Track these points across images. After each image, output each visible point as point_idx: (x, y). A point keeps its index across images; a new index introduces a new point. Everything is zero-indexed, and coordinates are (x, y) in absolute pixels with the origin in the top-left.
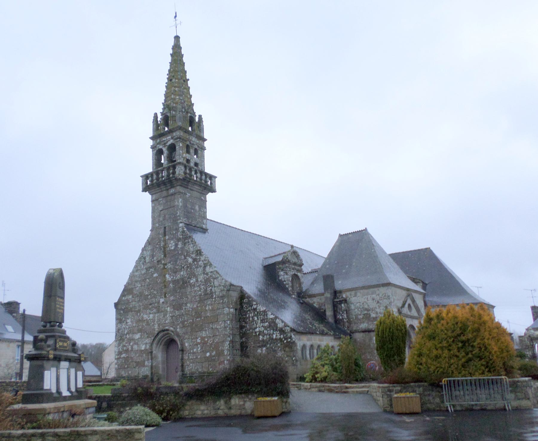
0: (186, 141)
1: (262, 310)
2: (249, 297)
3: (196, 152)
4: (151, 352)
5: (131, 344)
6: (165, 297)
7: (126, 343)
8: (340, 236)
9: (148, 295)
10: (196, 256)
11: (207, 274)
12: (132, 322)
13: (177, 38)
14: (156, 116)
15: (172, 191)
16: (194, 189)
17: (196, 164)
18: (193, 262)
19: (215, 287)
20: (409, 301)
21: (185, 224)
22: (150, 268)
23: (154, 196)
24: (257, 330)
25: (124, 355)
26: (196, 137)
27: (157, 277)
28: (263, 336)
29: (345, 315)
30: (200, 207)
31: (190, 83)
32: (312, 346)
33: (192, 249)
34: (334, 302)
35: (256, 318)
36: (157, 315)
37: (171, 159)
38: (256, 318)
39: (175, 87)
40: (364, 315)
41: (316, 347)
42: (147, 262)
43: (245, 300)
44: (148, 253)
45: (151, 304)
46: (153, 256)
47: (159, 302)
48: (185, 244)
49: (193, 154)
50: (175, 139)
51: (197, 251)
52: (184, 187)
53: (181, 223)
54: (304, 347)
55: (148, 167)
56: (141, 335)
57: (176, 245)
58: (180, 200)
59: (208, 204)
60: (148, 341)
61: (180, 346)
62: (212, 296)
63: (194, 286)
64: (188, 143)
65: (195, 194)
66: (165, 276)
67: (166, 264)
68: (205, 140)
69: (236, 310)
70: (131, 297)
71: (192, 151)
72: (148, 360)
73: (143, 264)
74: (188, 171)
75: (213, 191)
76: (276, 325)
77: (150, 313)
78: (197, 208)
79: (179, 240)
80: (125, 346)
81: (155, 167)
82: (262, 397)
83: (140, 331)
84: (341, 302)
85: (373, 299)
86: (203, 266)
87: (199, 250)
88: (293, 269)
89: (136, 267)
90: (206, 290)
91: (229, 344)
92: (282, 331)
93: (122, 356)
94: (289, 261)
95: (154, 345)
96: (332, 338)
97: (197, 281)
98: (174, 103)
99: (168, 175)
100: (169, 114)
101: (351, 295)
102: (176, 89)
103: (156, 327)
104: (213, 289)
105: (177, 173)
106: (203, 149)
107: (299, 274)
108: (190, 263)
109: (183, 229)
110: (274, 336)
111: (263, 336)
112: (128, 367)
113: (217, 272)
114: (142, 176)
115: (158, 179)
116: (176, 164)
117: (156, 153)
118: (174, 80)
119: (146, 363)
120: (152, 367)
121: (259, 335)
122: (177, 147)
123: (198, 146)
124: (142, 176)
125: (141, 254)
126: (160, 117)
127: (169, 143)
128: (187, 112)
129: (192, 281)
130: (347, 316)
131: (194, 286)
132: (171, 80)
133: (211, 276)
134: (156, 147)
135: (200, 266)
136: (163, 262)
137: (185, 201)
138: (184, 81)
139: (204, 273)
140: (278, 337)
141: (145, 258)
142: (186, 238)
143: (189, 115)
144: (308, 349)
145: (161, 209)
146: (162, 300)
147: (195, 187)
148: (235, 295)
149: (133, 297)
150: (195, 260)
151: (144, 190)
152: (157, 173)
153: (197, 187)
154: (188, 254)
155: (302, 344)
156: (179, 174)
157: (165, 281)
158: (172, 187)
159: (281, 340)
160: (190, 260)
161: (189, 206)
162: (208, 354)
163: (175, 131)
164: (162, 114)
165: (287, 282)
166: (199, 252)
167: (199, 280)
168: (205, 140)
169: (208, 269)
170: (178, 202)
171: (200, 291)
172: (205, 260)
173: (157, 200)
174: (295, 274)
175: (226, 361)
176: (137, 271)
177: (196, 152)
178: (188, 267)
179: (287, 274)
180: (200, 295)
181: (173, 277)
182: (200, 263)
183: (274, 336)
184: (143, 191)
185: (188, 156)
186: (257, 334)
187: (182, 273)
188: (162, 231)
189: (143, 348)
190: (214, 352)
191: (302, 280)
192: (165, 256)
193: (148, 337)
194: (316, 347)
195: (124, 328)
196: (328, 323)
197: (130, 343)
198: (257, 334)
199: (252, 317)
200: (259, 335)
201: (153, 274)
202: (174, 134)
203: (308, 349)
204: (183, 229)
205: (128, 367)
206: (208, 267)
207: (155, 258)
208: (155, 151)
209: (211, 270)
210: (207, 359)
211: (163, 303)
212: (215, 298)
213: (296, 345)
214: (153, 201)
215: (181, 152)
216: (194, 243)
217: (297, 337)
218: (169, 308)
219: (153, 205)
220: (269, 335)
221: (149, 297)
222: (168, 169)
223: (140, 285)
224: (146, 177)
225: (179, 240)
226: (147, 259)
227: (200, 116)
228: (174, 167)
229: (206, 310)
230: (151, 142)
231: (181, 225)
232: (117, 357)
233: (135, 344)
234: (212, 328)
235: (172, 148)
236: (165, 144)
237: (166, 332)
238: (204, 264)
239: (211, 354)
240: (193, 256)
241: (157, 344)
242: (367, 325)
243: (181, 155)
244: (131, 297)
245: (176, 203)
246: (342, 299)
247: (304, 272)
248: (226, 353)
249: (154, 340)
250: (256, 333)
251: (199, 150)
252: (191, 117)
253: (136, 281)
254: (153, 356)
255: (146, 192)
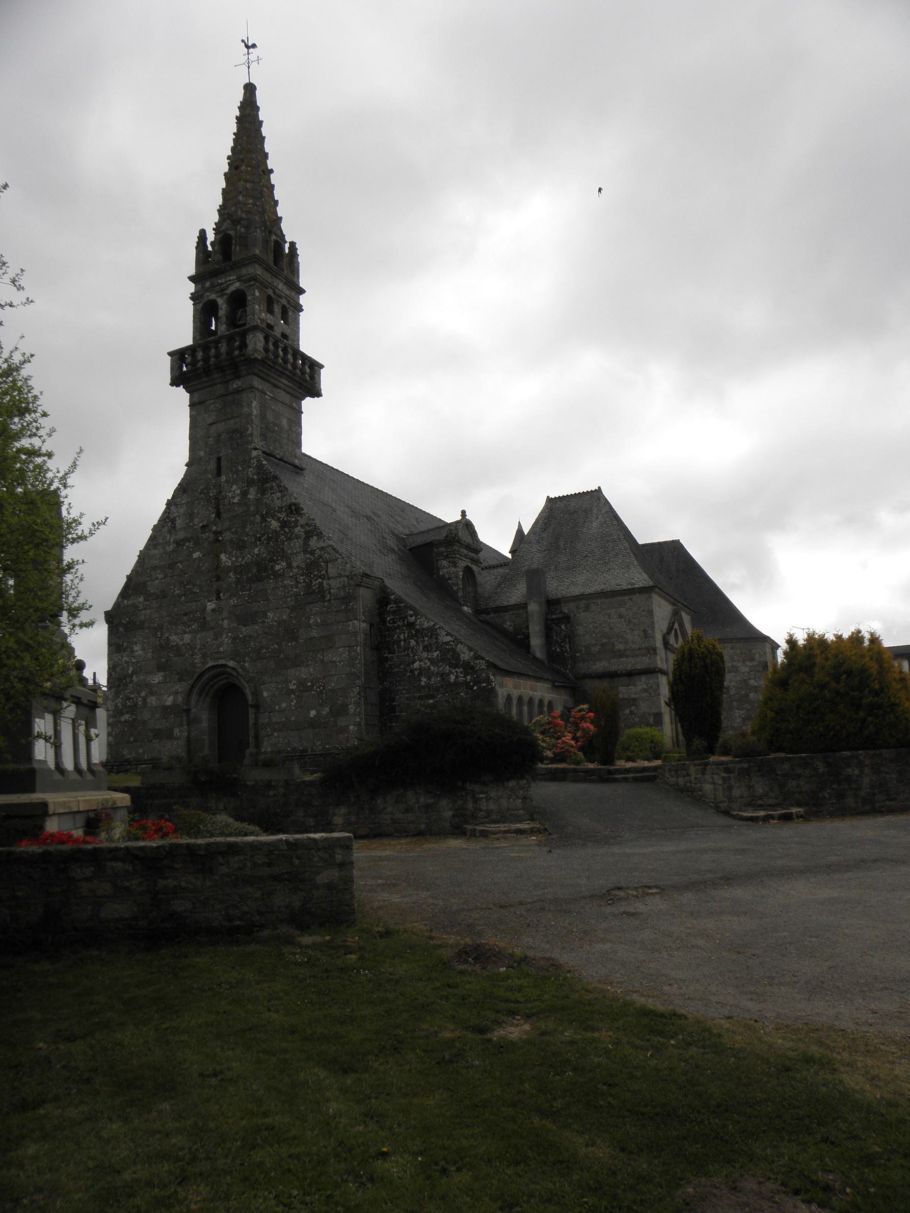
0: (267, 287)
1: (426, 625)
2: (399, 600)
3: (284, 315)
4: (188, 711)
5: (143, 694)
6: (218, 598)
7: (131, 693)
8: (549, 500)
9: (180, 596)
10: (287, 516)
11: (312, 553)
12: (143, 649)
13: (250, 89)
14: (202, 235)
15: (236, 384)
16: (281, 385)
17: (284, 336)
18: (282, 527)
19: (329, 579)
20: (676, 626)
21: (264, 452)
22: (187, 540)
23: (196, 395)
24: (416, 665)
25: (127, 717)
26: (285, 284)
27: (199, 558)
28: (429, 679)
29: (567, 646)
30: (290, 421)
31: (274, 179)
32: (520, 699)
33: (278, 503)
34: (546, 620)
35: (413, 643)
36: (199, 636)
37: (233, 320)
38: (413, 643)
39: (246, 181)
40: (602, 645)
41: (526, 699)
42: (178, 526)
43: (391, 607)
44: (182, 510)
45: (186, 614)
46: (191, 516)
47: (204, 609)
48: (263, 492)
49: (279, 316)
50: (245, 282)
51: (290, 506)
52: (262, 378)
53: (256, 449)
54: (509, 698)
55: (185, 338)
56: (165, 677)
57: (244, 494)
58: (255, 403)
59: (305, 419)
60: (181, 687)
61: (250, 698)
62: (323, 597)
63: (282, 575)
64: (270, 292)
65: (283, 396)
66: (217, 557)
67: (220, 533)
68: (302, 291)
69: (371, 625)
70: (141, 599)
71: (277, 309)
72: (181, 725)
73: (170, 532)
74: (271, 347)
75: (316, 393)
76: (456, 655)
77: (185, 633)
78: (285, 422)
79: (250, 483)
80: (129, 699)
81: (198, 337)
82: (236, 842)
83: (160, 668)
84: (559, 621)
85: (621, 616)
86: (303, 536)
87: (294, 504)
88: (466, 556)
89: (152, 539)
90: (309, 585)
91: (359, 693)
92: (468, 668)
93: (123, 719)
94: (459, 541)
95: (194, 697)
96: (548, 686)
97: (289, 566)
98: (242, 211)
99: (229, 353)
100: (232, 233)
101: (578, 607)
102: (248, 185)
103: (198, 659)
104: (325, 582)
105: (250, 348)
106: (299, 309)
107: (474, 568)
108: (275, 531)
109: (259, 461)
110: (453, 677)
111: (429, 679)
112: (136, 741)
113: (334, 549)
114: (170, 354)
115: (206, 359)
116: (249, 330)
117: (203, 308)
118: (243, 168)
119: (176, 732)
120: (189, 740)
121: (420, 674)
122: (249, 298)
123: (288, 302)
124: (170, 354)
125: (165, 512)
126: (211, 237)
127: (232, 288)
128: (270, 232)
129: (277, 567)
130: (570, 647)
131: (282, 575)
132: (237, 168)
133: (320, 557)
134: (202, 296)
135: (297, 537)
136: (214, 528)
137: (263, 407)
138: (263, 171)
139: (305, 551)
140: (461, 679)
141: (173, 521)
142: (266, 481)
143: (274, 237)
144: (515, 702)
145: (210, 421)
146: (210, 606)
147: (283, 380)
148: (365, 597)
149: (146, 600)
150: (284, 524)
151: (175, 382)
152: (206, 348)
153: (285, 382)
154: (271, 513)
155: (505, 694)
156: (256, 350)
157: (218, 567)
158: (238, 376)
159: (466, 684)
160: (275, 524)
161: (270, 417)
162: (313, 713)
163: (245, 265)
164: (217, 230)
165: (454, 581)
166: (295, 509)
167: (295, 564)
168: (302, 291)
169: (314, 542)
170: (250, 405)
171: (297, 587)
172: (307, 524)
173: (201, 403)
174: (467, 566)
175: (353, 729)
176: (155, 546)
177: (284, 315)
178: (269, 539)
179: (455, 565)
180: (297, 594)
181: (237, 557)
182: (297, 530)
183: (453, 677)
184: (172, 384)
185: (270, 319)
186: (416, 673)
187: (256, 551)
188: (213, 465)
189: (169, 701)
190: (327, 709)
191: (479, 579)
192: (218, 515)
193: (180, 680)
194: (526, 699)
195: (127, 663)
196: (535, 658)
197: (139, 693)
198: (416, 673)
199: (404, 641)
200: (420, 674)
201: (191, 553)
202: (244, 271)
203: (515, 702)
204: (259, 461)
205: (136, 741)
206: (315, 538)
207: (196, 521)
208: (201, 305)
209: (321, 544)
210: (313, 724)
211: (213, 610)
212: (329, 600)
213: (496, 696)
214: (192, 405)
215: (257, 307)
216: (283, 490)
217: (499, 678)
218: (226, 622)
219: (194, 413)
220: (442, 675)
221: (183, 598)
222: (230, 339)
223: (161, 576)
224: (178, 356)
225: (250, 483)
226: (179, 523)
227: (293, 244)
228: (243, 335)
229: (310, 626)
230: (191, 287)
231: (254, 453)
232: (111, 720)
233: (152, 693)
234: (322, 661)
235: (238, 301)
236: (222, 290)
237: (219, 670)
238: (306, 532)
239: (318, 712)
240: (282, 516)
241: (200, 695)
242: (607, 665)
243: (257, 312)
244: (141, 599)
245: (246, 409)
246: (560, 616)
247: (485, 564)
248: (352, 711)
249: (193, 686)
250: (412, 671)
251: (290, 310)
252: (276, 242)
253: (154, 568)
254: (192, 716)
255: (178, 386)
